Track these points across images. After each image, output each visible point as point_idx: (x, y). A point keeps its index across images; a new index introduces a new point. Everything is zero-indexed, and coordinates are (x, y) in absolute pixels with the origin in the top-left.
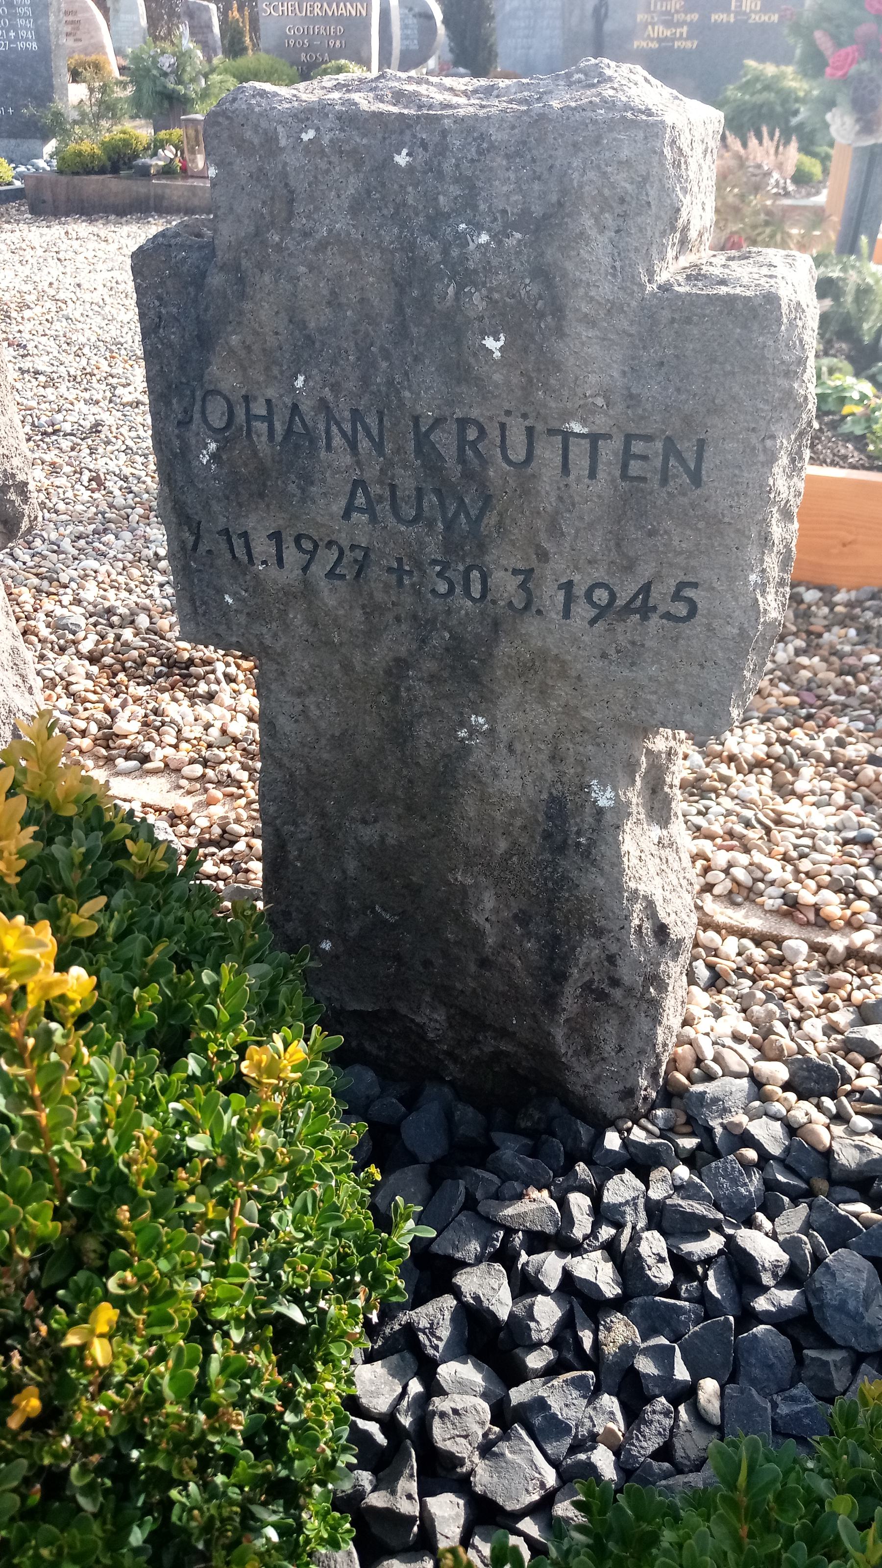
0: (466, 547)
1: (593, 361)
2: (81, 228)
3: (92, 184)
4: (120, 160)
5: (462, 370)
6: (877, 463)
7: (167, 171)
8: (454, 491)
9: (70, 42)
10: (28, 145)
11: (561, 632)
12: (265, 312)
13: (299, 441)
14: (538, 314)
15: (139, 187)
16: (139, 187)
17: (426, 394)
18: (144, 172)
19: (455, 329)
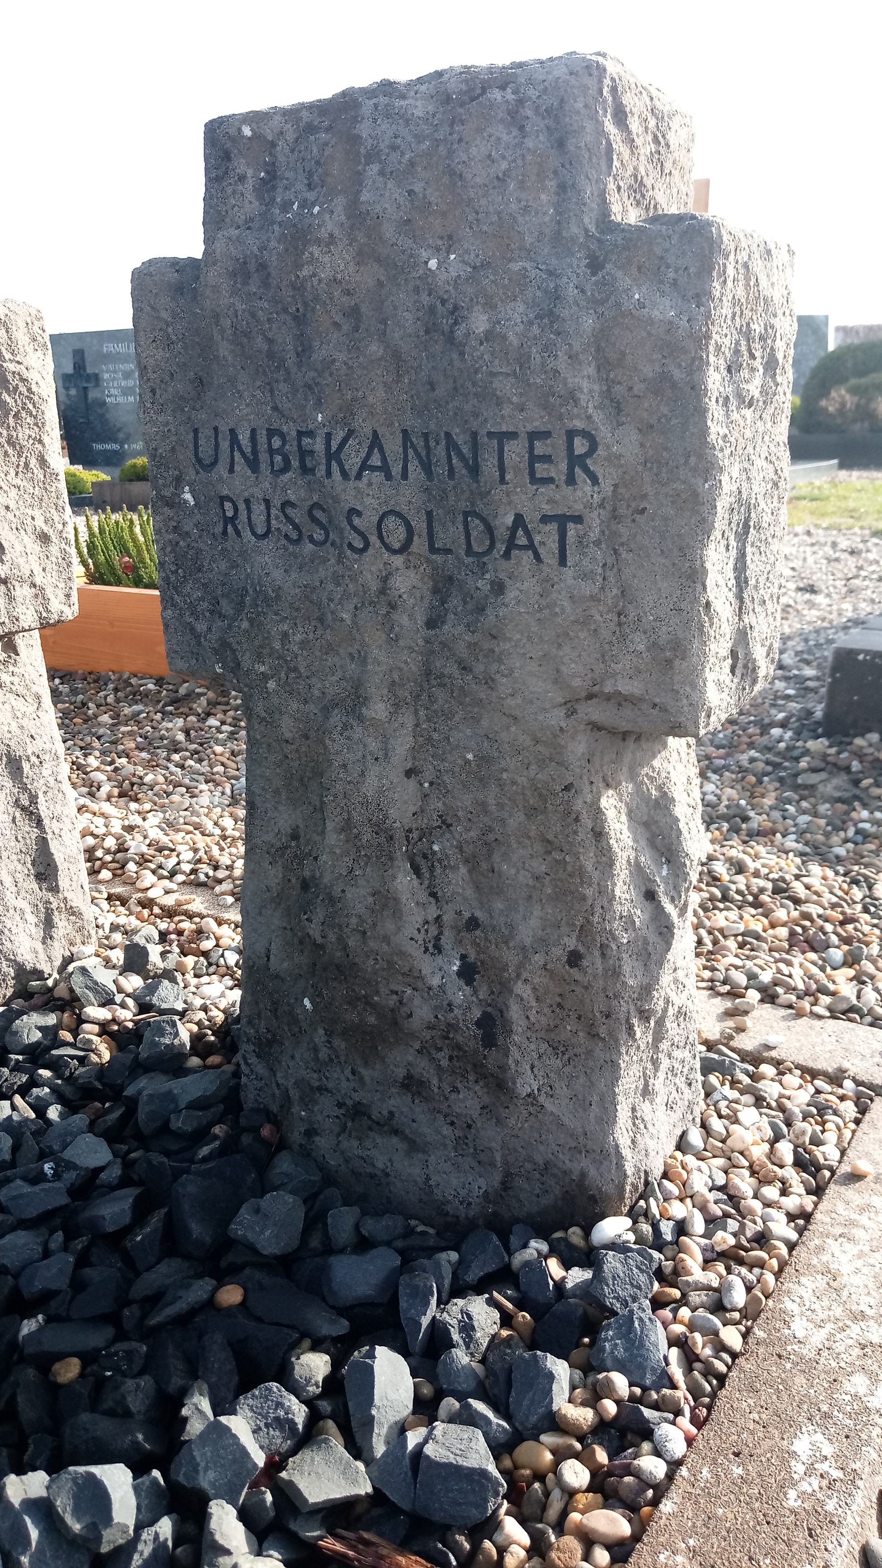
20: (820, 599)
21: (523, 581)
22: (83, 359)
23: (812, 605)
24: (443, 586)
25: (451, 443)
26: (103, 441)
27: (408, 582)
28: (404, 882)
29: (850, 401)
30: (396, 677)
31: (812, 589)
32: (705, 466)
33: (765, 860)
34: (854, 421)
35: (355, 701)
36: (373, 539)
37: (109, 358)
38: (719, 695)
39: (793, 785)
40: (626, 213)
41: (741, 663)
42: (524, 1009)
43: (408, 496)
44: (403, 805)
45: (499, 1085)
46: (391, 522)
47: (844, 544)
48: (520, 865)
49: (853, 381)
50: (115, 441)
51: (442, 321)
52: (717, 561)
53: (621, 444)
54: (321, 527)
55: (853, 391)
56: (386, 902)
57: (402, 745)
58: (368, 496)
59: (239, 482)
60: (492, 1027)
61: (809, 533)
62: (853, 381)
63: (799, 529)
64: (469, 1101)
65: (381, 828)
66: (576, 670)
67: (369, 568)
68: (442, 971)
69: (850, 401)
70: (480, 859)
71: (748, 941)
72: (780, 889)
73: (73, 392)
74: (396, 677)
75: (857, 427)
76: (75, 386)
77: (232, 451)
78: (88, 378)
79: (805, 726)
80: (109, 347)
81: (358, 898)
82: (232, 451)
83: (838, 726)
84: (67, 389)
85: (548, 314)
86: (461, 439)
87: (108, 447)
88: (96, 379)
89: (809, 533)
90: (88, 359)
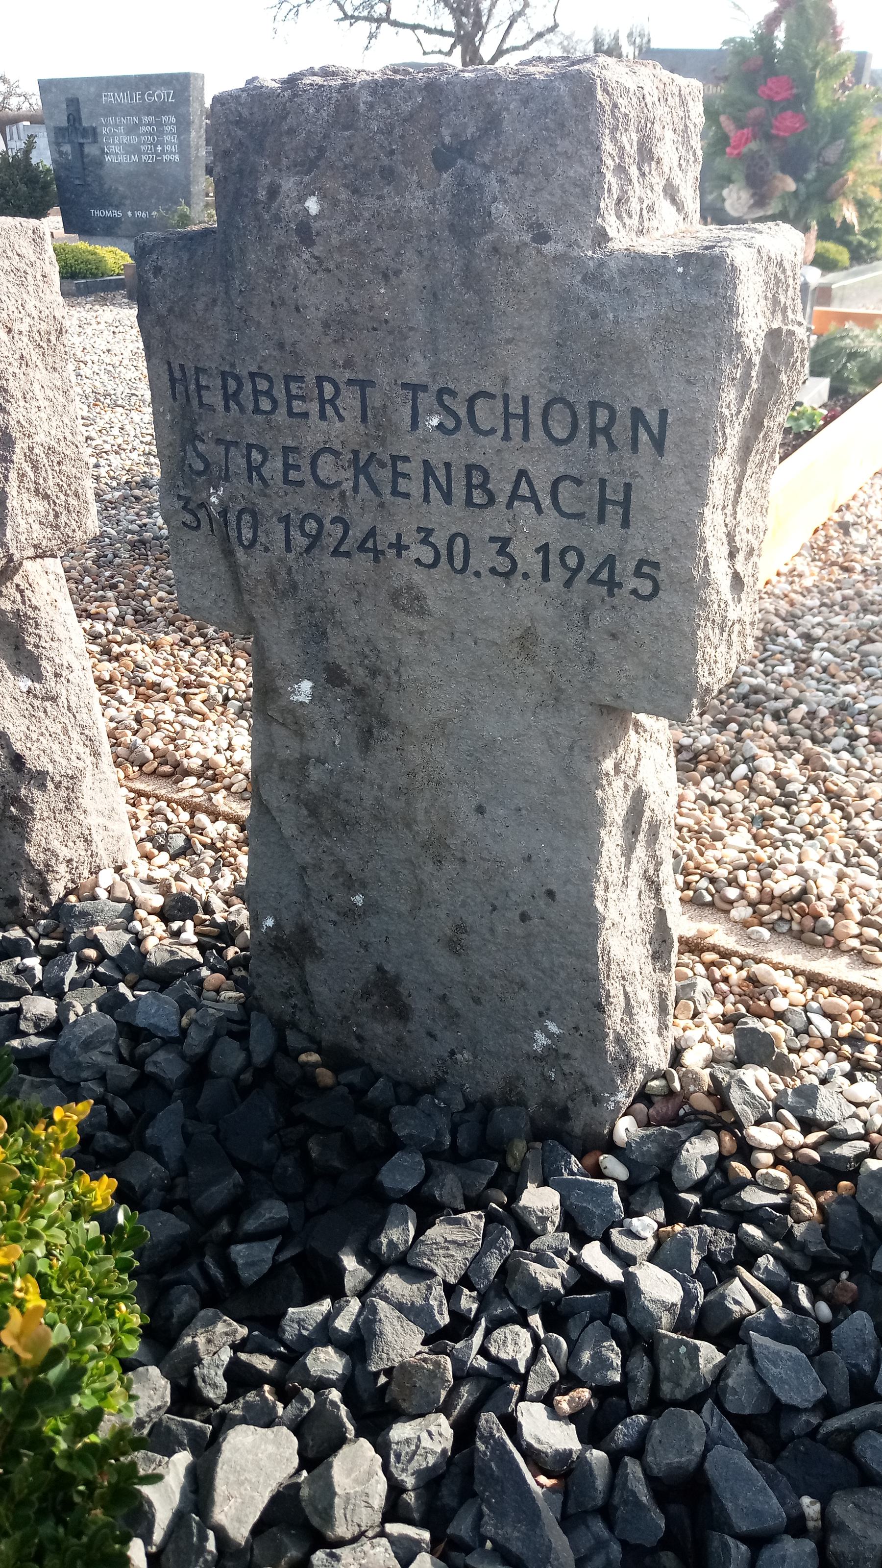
22: (78, 111)
25: (447, 497)
26: (102, 207)
30: (698, 1153)
36: (444, 558)
37: (111, 111)
46: (560, 433)
50: (117, 208)
73: (67, 148)
74: (698, 1153)
76: (70, 142)
77: (635, 430)
78: (85, 132)
80: (109, 98)
82: (635, 430)
84: (58, 144)
86: (652, 416)
87: (109, 214)
88: (93, 133)
90: (84, 113)
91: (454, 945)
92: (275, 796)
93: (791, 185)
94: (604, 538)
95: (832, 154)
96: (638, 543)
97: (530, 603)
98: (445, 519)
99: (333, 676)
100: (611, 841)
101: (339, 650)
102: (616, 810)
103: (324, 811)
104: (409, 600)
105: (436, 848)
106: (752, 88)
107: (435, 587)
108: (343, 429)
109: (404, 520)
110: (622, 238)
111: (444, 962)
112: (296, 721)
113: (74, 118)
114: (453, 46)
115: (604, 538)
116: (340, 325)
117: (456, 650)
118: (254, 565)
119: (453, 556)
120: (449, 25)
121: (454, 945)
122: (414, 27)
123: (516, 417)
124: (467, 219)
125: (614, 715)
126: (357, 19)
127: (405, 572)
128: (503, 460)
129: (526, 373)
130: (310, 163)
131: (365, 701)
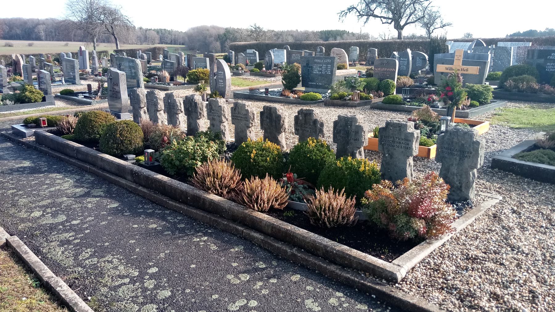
0: (348, 137)
1: (353, 128)
2: (333, 109)
3: (335, 101)
4: (342, 97)
5: (348, 128)
6: (552, 162)
7: (350, 99)
8: (348, 133)
9: (338, 60)
10: (325, 90)
11: (352, 141)
12: (339, 125)
13: (340, 131)
14: (351, 126)
15: (344, 102)
16: (344, 102)
17: (346, 129)
18: (345, 100)
19: (348, 126)
20: (495, 145)
21: (466, 159)
23: (493, 146)
24: (460, 159)
27: (458, 158)
28: (455, 177)
29: (513, 83)
31: (494, 142)
32: (479, 154)
33: (482, 181)
34: (514, 88)
35: (452, 165)
37: (316, 63)
38: (479, 166)
39: (485, 174)
40: (475, 140)
41: (480, 164)
42: (464, 185)
43: (459, 153)
44: (455, 172)
45: (461, 191)
47: (503, 131)
48: (464, 176)
49: (514, 77)
51: (463, 145)
52: (479, 159)
53: (474, 153)
54: (452, 154)
55: (514, 81)
56: (454, 178)
57: (456, 168)
58: (456, 153)
59: (445, 150)
60: (461, 187)
61: (496, 127)
62: (514, 77)
63: (494, 126)
64: (458, 192)
65: (454, 173)
66: (469, 164)
67: (455, 157)
68: (457, 183)
69: (513, 83)
70: (461, 176)
71: (480, 188)
72: (483, 184)
75: (514, 90)
78: (310, 67)
79: (488, 167)
81: (451, 178)
83: (492, 167)
85: (470, 146)
89: (496, 127)
91: (396, 173)
92: (384, 163)
93: (451, 102)
94: (407, 146)
95: (457, 98)
96: (409, 146)
97: (403, 150)
98: (398, 145)
99: (389, 154)
100: (408, 166)
101: (390, 152)
102: (408, 163)
103: (388, 164)
104: (395, 149)
105: (395, 166)
106: (445, 88)
107: (397, 149)
108: (392, 139)
109: (395, 145)
110: (408, 131)
111: (396, 175)
112: (386, 157)
113: (308, 64)
114: (392, 22)
115: (407, 146)
116: (392, 134)
117: (398, 152)
118: (385, 147)
119: (398, 147)
120: (391, 16)
121: (396, 173)
122: (380, 17)
123: (402, 139)
124: (400, 130)
125: (408, 157)
126: (364, 15)
127: (395, 148)
128: (401, 142)
129: (403, 137)
130: (391, 126)
131: (391, 156)
